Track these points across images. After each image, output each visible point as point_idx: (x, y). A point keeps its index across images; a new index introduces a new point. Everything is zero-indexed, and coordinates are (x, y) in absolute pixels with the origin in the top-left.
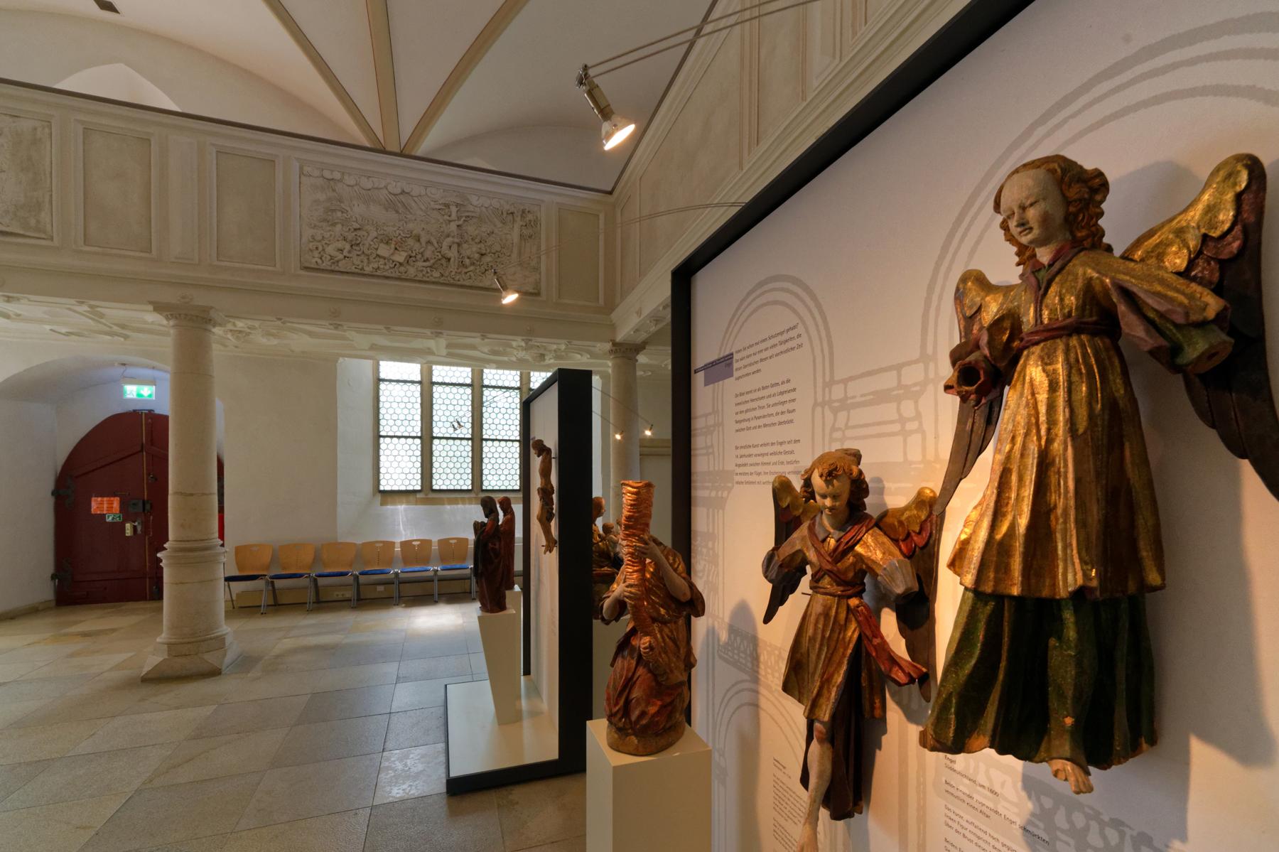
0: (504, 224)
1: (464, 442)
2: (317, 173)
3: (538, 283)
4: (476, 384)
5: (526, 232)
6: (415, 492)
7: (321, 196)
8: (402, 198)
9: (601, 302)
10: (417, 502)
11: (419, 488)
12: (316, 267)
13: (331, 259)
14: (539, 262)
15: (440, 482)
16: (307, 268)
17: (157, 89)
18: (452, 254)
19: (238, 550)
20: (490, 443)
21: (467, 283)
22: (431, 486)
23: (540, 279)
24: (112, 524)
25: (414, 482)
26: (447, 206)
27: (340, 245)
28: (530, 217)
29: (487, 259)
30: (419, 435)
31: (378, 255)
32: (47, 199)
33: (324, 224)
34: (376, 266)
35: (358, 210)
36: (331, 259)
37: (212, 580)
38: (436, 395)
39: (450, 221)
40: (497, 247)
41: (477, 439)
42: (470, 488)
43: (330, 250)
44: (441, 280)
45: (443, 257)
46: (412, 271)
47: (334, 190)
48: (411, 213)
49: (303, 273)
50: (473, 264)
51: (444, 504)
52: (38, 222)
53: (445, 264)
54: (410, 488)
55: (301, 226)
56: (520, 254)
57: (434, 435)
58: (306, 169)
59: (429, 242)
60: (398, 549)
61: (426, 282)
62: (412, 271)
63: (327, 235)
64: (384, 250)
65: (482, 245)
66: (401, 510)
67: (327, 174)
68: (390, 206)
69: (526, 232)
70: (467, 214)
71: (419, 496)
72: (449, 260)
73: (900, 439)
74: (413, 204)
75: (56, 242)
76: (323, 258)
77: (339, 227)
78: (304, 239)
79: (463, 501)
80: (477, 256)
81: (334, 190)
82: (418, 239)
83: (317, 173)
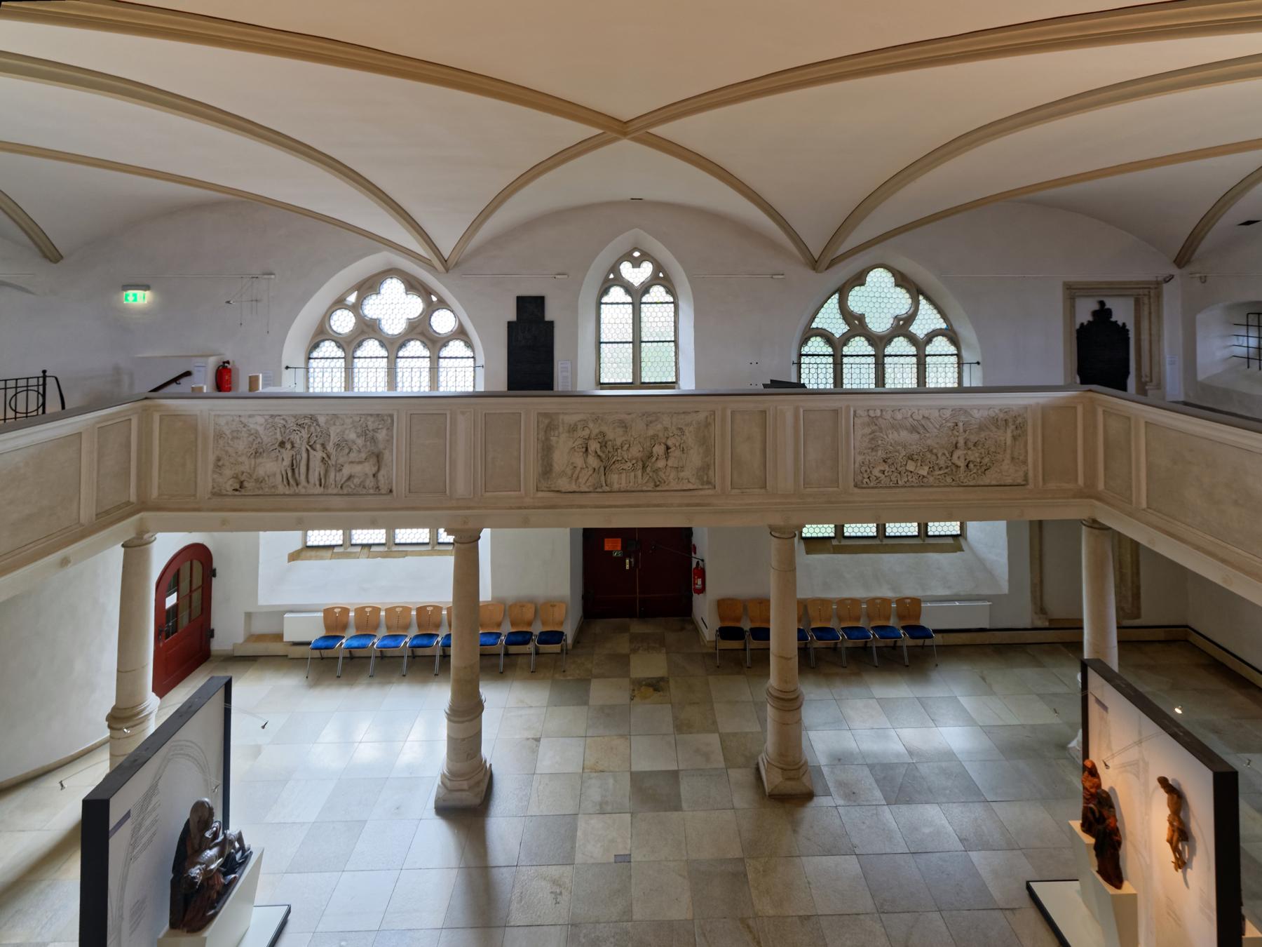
0: (998, 428)
6: (829, 538)
7: (867, 430)
9: (1081, 481)
12: (866, 486)
13: (877, 479)
14: (1026, 456)
15: (668, 310)
17: (675, 260)
21: (971, 484)
22: (843, 533)
23: (1027, 470)
24: (617, 558)
32: (712, 461)
35: (893, 436)
36: (877, 479)
40: (993, 449)
42: (875, 534)
47: (876, 425)
48: (928, 432)
53: (954, 470)
54: (826, 535)
55: (855, 454)
56: (1012, 452)
64: (911, 466)
67: (872, 413)
68: (913, 429)
71: (835, 542)
72: (958, 467)
73: (1257, 336)
74: (930, 424)
76: (871, 479)
81: (876, 425)
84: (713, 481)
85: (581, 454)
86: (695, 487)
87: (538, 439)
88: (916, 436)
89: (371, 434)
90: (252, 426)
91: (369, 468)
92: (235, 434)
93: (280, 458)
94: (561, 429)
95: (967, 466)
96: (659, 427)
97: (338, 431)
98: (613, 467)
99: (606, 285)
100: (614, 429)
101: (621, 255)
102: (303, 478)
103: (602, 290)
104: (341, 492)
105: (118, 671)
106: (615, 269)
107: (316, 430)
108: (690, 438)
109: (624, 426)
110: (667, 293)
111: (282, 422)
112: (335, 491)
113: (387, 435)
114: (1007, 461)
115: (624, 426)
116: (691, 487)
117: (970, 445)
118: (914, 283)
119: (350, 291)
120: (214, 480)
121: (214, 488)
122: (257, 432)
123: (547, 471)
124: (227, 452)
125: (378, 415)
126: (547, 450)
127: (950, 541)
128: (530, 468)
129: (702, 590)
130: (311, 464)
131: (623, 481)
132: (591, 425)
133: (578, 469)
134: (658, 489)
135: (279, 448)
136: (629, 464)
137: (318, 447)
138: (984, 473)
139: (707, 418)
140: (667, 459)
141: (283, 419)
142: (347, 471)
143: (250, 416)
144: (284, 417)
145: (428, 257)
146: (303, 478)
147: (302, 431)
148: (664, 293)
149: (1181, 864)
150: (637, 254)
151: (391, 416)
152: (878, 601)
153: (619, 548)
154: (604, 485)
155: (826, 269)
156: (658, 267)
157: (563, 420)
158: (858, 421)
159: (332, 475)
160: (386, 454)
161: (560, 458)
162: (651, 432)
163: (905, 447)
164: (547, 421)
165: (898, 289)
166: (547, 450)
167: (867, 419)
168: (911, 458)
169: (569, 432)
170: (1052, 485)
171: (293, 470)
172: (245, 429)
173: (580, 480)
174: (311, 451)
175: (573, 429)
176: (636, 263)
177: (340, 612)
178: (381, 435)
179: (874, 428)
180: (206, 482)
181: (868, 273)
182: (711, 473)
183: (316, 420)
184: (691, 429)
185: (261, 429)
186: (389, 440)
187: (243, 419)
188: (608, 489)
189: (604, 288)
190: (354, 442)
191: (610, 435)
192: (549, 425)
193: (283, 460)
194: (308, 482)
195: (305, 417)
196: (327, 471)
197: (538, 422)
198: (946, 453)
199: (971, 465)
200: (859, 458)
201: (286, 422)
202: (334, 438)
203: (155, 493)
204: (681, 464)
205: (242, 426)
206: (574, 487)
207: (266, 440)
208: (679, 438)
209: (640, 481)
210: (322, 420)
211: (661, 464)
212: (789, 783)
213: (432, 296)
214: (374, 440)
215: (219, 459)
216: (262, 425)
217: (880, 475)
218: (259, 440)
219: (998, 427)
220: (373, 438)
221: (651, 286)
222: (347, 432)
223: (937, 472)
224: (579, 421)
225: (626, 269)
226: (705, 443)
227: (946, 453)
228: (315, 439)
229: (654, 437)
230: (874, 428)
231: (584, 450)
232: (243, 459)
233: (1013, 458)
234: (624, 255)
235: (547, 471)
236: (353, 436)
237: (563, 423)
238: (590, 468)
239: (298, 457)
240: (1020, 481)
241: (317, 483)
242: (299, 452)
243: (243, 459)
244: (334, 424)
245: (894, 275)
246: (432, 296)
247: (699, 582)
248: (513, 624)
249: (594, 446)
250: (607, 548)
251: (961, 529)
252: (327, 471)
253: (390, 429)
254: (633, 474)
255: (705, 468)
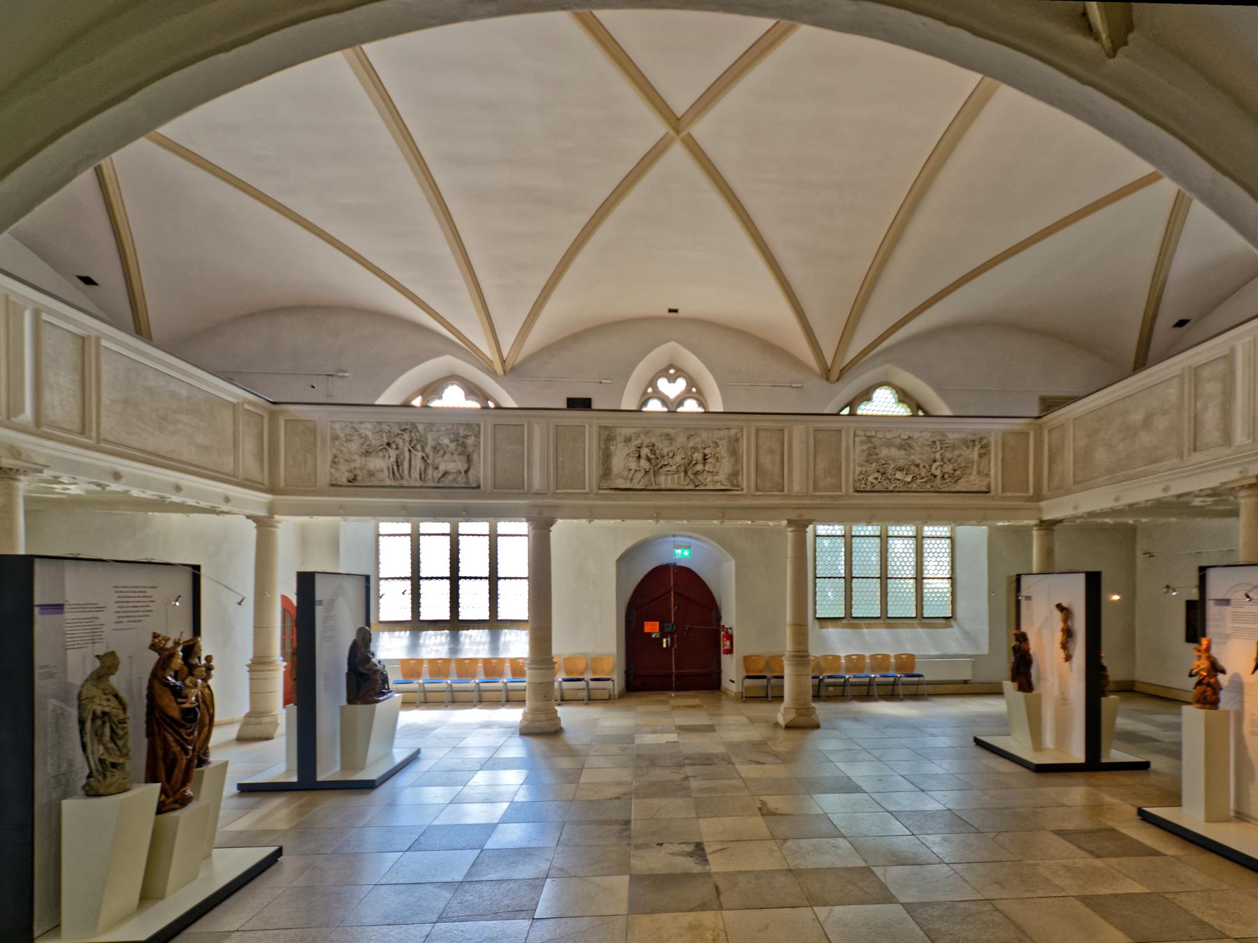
1: (875, 580)
2: (863, 434)
3: (989, 485)
4: (884, 535)
5: (983, 451)
7: (865, 447)
8: (909, 441)
10: (845, 626)
11: (843, 616)
14: (989, 470)
16: (858, 491)
18: (938, 473)
19: (747, 660)
20: (892, 581)
24: (655, 639)
25: (840, 611)
26: (934, 442)
27: (876, 475)
28: (984, 442)
29: (958, 473)
30: (843, 576)
31: (896, 479)
33: (866, 463)
34: (895, 485)
35: (884, 452)
37: (265, 679)
38: (854, 545)
39: (936, 452)
40: (963, 464)
41: (884, 578)
42: (879, 615)
43: (871, 479)
44: (932, 490)
45: (932, 474)
46: (914, 486)
49: (855, 494)
50: (949, 477)
51: (862, 628)
52: (737, 482)
56: (978, 466)
57: (853, 576)
58: (858, 433)
59: (924, 467)
60: (868, 661)
61: (922, 492)
62: (914, 486)
63: (868, 469)
64: (899, 475)
65: (955, 464)
66: (832, 632)
67: (868, 434)
69: (983, 451)
70: (946, 445)
71: (844, 621)
72: (935, 476)
75: (745, 491)
77: (874, 464)
78: (856, 474)
79: (876, 626)
80: (952, 471)
82: (917, 466)
83: (863, 434)
84: (741, 484)
85: (635, 458)
86: (726, 488)
87: (599, 447)
88: (903, 452)
89: (461, 440)
90: (362, 431)
91: (461, 466)
92: (349, 437)
93: (387, 456)
94: (618, 439)
95: (943, 476)
96: (698, 439)
97: (434, 436)
98: (661, 470)
99: (646, 397)
100: (662, 440)
101: (659, 370)
102: (406, 472)
103: (641, 402)
104: (438, 485)
105: (255, 627)
106: (652, 383)
107: (416, 435)
108: (723, 451)
109: (670, 438)
110: (699, 405)
111: (387, 427)
112: (433, 485)
113: (476, 441)
114: (974, 473)
115: (670, 438)
116: (724, 488)
117: (946, 460)
118: (915, 399)
119: (414, 396)
120: (331, 474)
121: (331, 480)
122: (366, 436)
123: (607, 472)
124: (341, 451)
125: (467, 425)
126: (606, 457)
127: (943, 621)
128: (591, 469)
129: (730, 651)
130: (413, 463)
131: (669, 482)
132: (643, 437)
133: (632, 471)
134: (697, 488)
135: (387, 447)
136: (675, 467)
137: (419, 447)
138: (956, 481)
139: (736, 434)
140: (704, 464)
141: (389, 425)
142: (442, 468)
143: (361, 423)
144: (389, 424)
145: (490, 358)
146: (406, 472)
147: (405, 434)
148: (697, 405)
149: (1068, 658)
150: (672, 371)
151: (478, 425)
152: (880, 656)
153: (657, 630)
154: (654, 484)
155: (838, 380)
156: (691, 382)
157: (620, 433)
158: (857, 439)
159: (430, 471)
160: (475, 457)
161: (619, 462)
162: (691, 444)
163: (894, 461)
164: (606, 433)
165: (901, 405)
166: (606, 457)
167: (864, 438)
168: (900, 469)
169: (625, 441)
170: (1006, 494)
171: (398, 466)
172: (356, 433)
173: (634, 481)
174: (413, 451)
175: (628, 440)
176: (672, 379)
177: (414, 663)
178: (470, 441)
179: (870, 445)
180: (324, 473)
181: (875, 389)
182: (740, 478)
183: (416, 427)
184: (724, 442)
185: (370, 434)
186: (477, 445)
187: (354, 425)
188: (656, 487)
189: (643, 400)
190: (447, 446)
191: (659, 445)
192: (607, 438)
193: (389, 456)
194: (410, 476)
195: (407, 424)
196: (425, 469)
197: (600, 434)
198: (927, 466)
199: (946, 476)
200: (858, 470)
201: (391, 428)
202: (431, 443)
203: (282, 484)
204: (715, 470)
205: (353, 430)
206: (628, 486)
207: (374, 442)
208: (714, 449)
209: (682, 482)
210: (421, 428)
211: (699, 467)
212: (802, 718)
213: (489, 402)
214: (464, 445)
215: (335, 457)
216: (370, 430)
217: (874, 481)
218: (369, 442)
219: (968, 447)
220: (463, 443)
221: (685, 399)
222: (442, 438)
223: (919, 481)
224: (634, 433)
225: (663, 384)
226: (734, 453)
227: (927, 466)
228: (415, 442)
229: (695, 449)
230: (870, 445)
231: (637, 455)
232: (356, 457)
233: (979, 472)
234: (660, 372)
235: (607, 472)
236: (446, 441)
237: (620, 435)
238: (642, 470)
239: (402, 457)
240: (984, 489)
241: (418, 478)
242: (402, 453)
243: (356, 457)
244: (431, 431)
245: (897, 393)
246: (489, 402)
247: (728, 643)
248: (567, 673)
249: (645, 451)
250: (646, 630)
251: (952, 612)
252: (425, 469)
253: (477, 436)
254: (676, 476)
255: (735, 474)
